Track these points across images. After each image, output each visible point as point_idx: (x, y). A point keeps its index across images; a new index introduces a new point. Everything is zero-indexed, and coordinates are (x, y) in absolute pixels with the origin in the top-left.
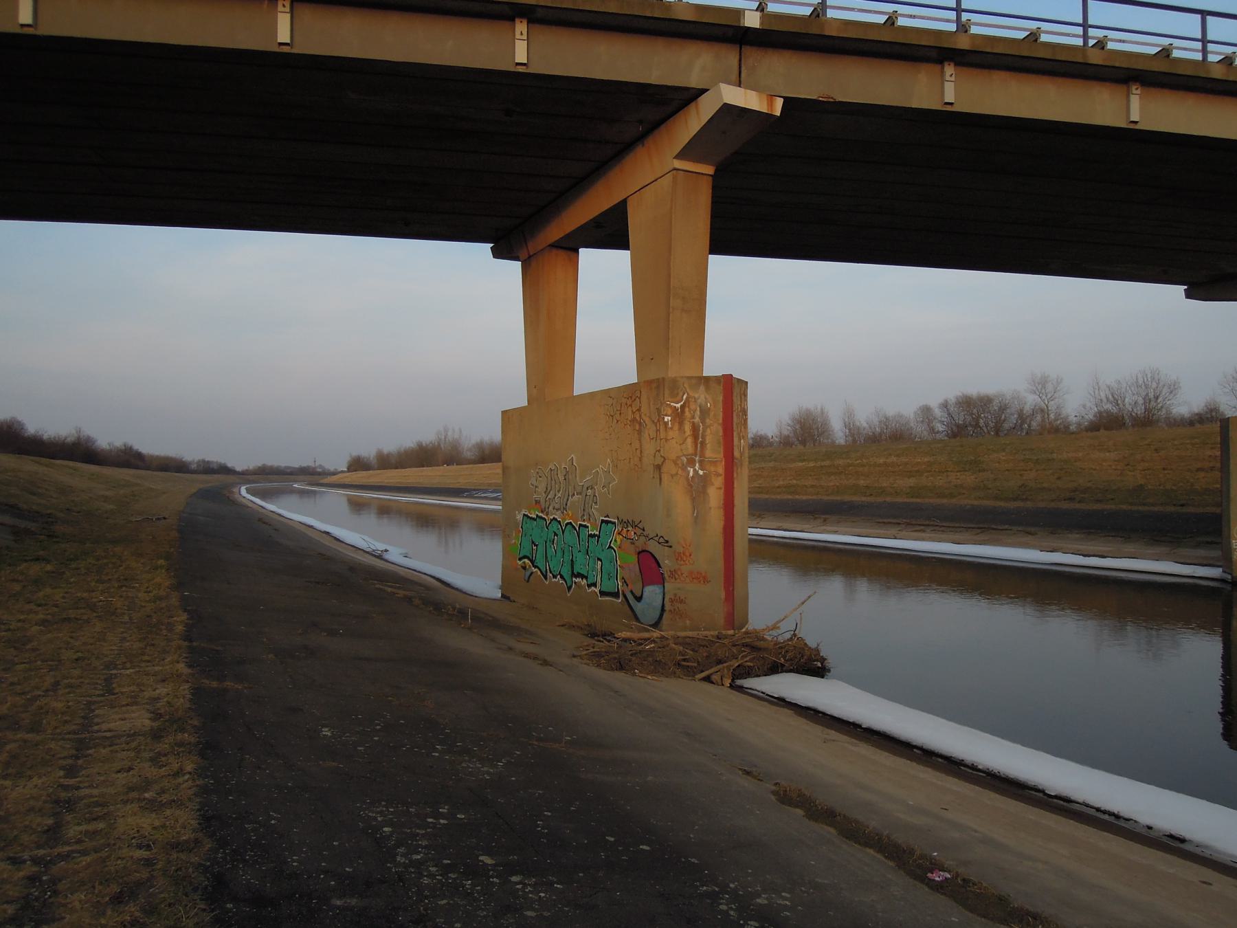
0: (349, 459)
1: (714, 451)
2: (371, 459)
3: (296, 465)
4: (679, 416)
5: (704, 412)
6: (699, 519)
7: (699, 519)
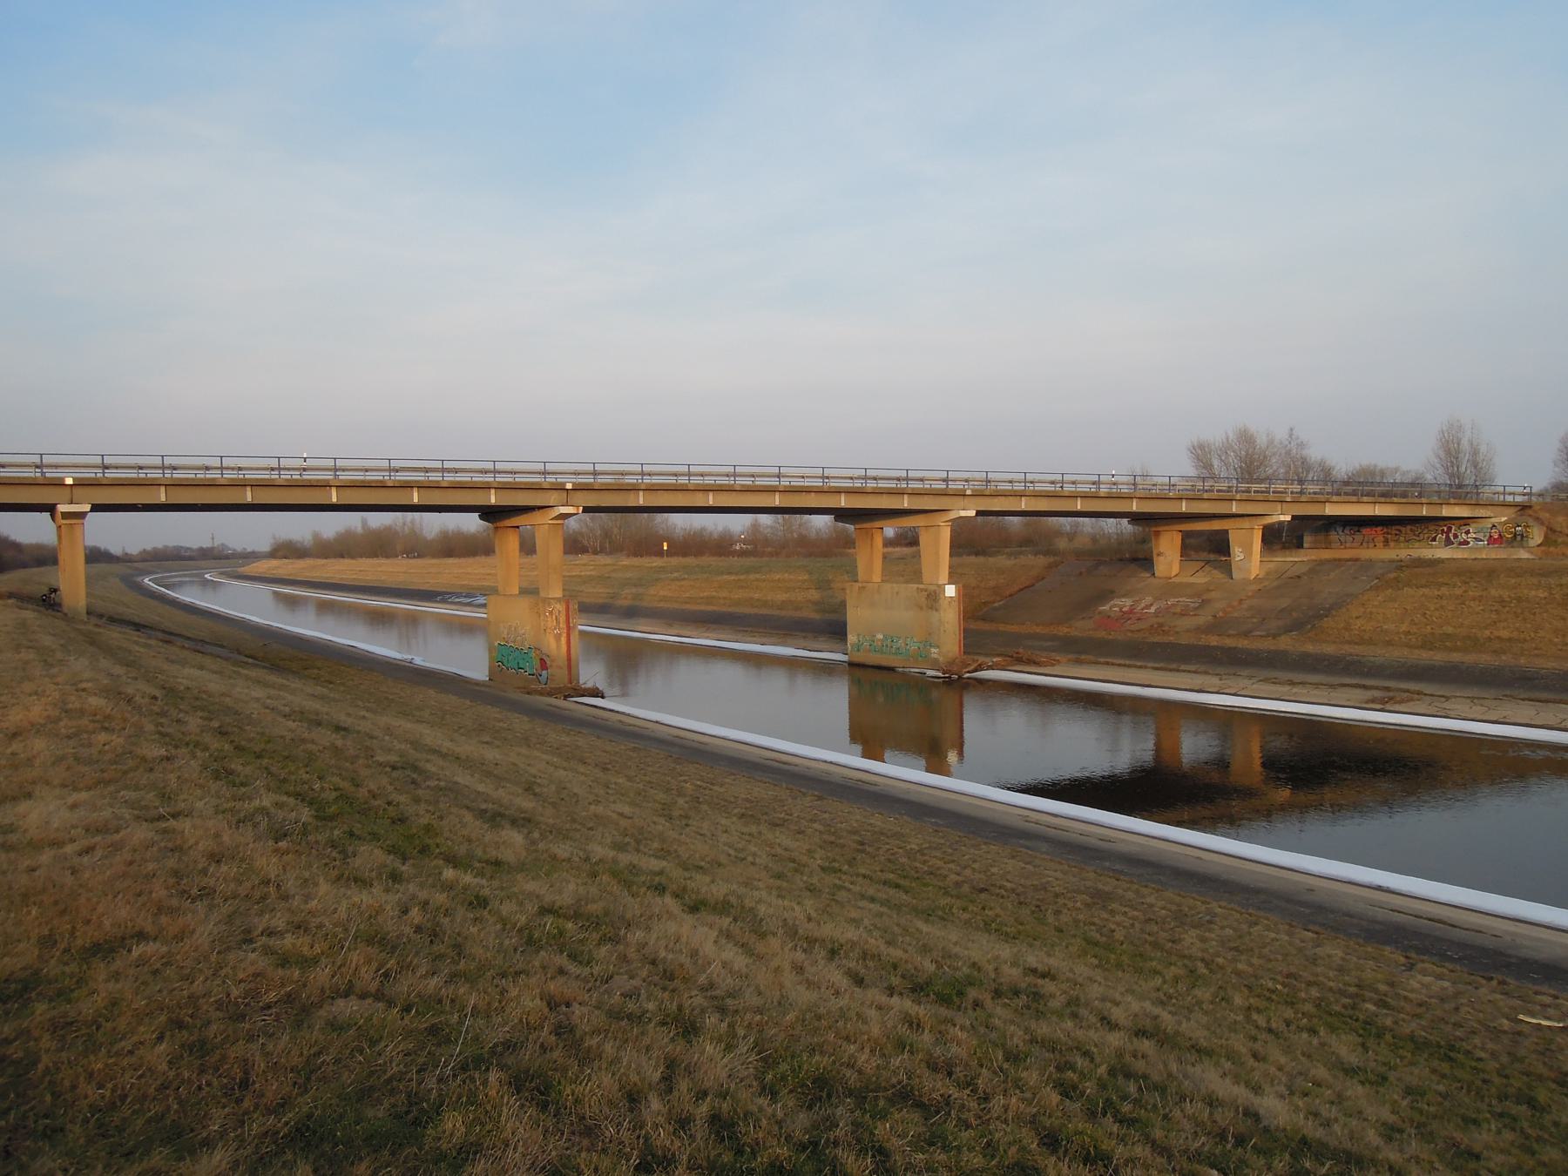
0: (272, 541)
1: (563, 625)
4: (551, 613)
6: (558, 646)
7: (558, 646)
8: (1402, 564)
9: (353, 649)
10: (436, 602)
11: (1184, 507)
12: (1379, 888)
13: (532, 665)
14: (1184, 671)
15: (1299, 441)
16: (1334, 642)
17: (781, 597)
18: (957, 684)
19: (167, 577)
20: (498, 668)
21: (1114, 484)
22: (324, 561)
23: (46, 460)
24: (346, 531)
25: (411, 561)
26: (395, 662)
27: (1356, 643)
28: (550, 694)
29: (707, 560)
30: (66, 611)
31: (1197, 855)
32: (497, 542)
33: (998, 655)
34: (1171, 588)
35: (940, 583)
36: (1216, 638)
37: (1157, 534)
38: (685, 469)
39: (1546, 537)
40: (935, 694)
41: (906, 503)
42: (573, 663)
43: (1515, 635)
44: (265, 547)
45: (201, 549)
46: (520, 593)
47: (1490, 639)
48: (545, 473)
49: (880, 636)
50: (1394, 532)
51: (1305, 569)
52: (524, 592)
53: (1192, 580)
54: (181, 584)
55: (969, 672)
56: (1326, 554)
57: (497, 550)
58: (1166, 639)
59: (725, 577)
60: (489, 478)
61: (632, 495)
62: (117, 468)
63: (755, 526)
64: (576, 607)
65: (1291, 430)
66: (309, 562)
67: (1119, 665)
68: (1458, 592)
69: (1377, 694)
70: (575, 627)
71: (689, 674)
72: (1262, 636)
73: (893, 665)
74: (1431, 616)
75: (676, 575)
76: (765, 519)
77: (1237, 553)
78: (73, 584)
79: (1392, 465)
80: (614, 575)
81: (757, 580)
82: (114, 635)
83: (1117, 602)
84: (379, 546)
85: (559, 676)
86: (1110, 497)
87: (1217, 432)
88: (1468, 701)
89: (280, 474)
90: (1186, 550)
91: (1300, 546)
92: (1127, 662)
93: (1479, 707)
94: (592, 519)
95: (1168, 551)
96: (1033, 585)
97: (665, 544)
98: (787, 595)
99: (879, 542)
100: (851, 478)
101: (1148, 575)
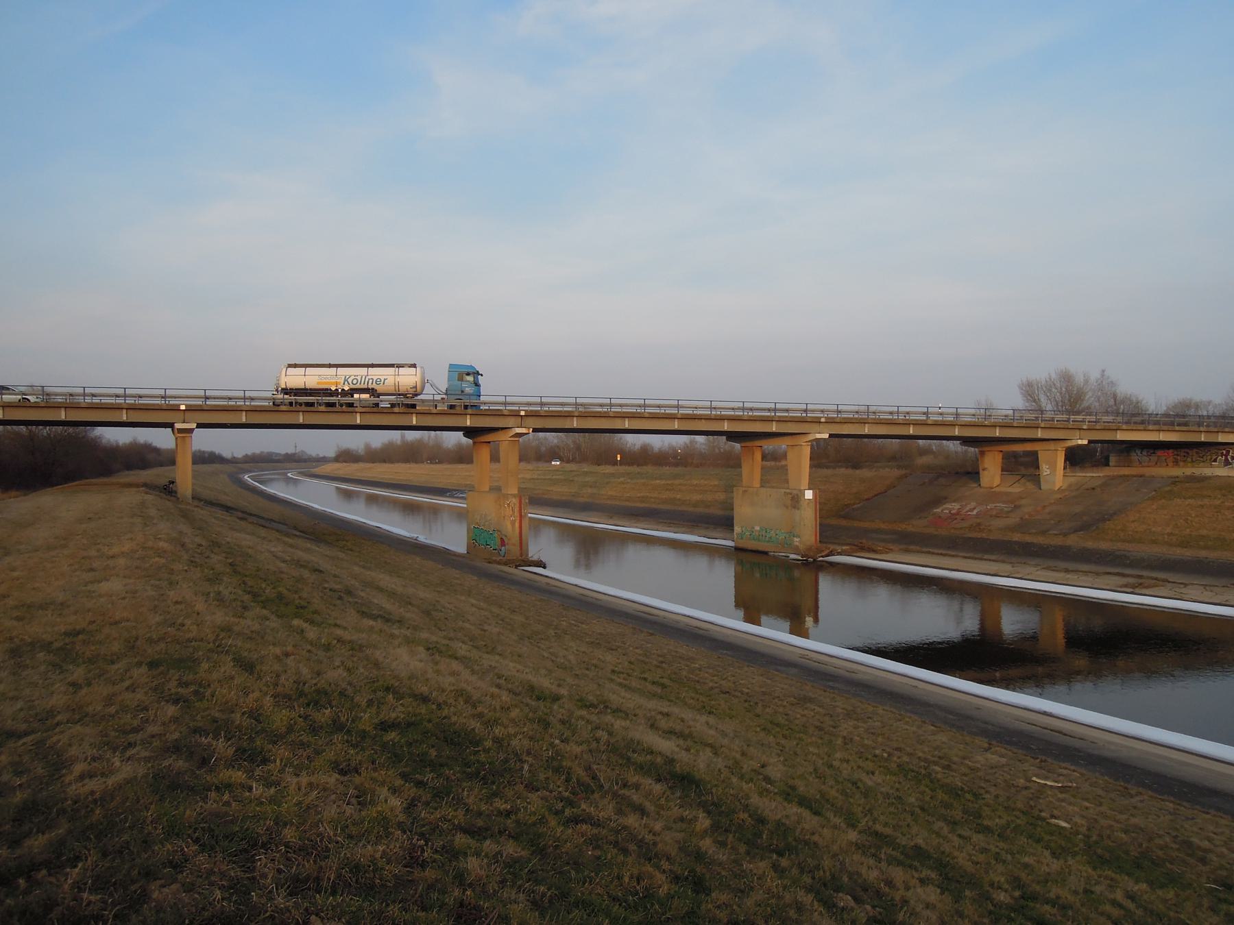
1: (517, 514)
2: (360, 451)
3: (283, 452)
5: (515, 504)
8: (1177, 480)
9: (379, 530)
10: (447, 496)
11: (998, 433)
12: (1045, 713)
14: (986, 560)
15: (1110, 380)
16: (1111, 540)
17: (696, 497)
18: (813, 565)
19: (263, 475)
20: (472, 545)
21: (941, 414)
22: (371, 465)
24: (389, 443)
25: (432, 466)
26: (405, 539)
27: (1128, 542)
28: (506, 564)
29: (649, 469)
30: (179, 496)
31: (914, 684)
32: (474, 455)
34: (993, 496)
35: (802, 488)
37: (982, 453)
38: (608, 401)
40: (796, 573)
41: (774, 428)
42: (524, 542)
44: (331, 454)
46: (490, 489)
49: (757, 528)
50: (1182, 454)
52: (492, 489)
53: (1010, 490)
54: (272, 480)
55: (822, 557)
56: (1126, 471)
57: (474, 459)
58: (979, 535)
59: (658, 481)
60: (120, 401)
62: (214, 398)
63: (691, 442)
64: (527, 501)
65: (1103, 371)
66: (361, 465)
67: (938, 554)
68: (1218, 502)
69: (1131, 580)
70: (526, 514)
71: (634, 554)
72: (1056, 535)
73: (766, 550)
74: (1191, 521)
75: (622, 479)
76: (700, 439)
77: (1045, 470)
78: (185, 477)
80: (576, 479)
82: (202, 513)
83: (948, 506)
84: (410, 454)
85: (514, 551)
86: (936, 424)
87: (1042, 372)
88: (1202, 588)
89: (125, 400)
91: (1107, 465)
92: (944, 552)
93: (1210, 593)
94: (566, 436)
95: (992, 469)
96: (886, 492)
97: (619, 456)
98: (701, 496)
99: (758, 456)
100: (733, 409)
101: (976, 485)
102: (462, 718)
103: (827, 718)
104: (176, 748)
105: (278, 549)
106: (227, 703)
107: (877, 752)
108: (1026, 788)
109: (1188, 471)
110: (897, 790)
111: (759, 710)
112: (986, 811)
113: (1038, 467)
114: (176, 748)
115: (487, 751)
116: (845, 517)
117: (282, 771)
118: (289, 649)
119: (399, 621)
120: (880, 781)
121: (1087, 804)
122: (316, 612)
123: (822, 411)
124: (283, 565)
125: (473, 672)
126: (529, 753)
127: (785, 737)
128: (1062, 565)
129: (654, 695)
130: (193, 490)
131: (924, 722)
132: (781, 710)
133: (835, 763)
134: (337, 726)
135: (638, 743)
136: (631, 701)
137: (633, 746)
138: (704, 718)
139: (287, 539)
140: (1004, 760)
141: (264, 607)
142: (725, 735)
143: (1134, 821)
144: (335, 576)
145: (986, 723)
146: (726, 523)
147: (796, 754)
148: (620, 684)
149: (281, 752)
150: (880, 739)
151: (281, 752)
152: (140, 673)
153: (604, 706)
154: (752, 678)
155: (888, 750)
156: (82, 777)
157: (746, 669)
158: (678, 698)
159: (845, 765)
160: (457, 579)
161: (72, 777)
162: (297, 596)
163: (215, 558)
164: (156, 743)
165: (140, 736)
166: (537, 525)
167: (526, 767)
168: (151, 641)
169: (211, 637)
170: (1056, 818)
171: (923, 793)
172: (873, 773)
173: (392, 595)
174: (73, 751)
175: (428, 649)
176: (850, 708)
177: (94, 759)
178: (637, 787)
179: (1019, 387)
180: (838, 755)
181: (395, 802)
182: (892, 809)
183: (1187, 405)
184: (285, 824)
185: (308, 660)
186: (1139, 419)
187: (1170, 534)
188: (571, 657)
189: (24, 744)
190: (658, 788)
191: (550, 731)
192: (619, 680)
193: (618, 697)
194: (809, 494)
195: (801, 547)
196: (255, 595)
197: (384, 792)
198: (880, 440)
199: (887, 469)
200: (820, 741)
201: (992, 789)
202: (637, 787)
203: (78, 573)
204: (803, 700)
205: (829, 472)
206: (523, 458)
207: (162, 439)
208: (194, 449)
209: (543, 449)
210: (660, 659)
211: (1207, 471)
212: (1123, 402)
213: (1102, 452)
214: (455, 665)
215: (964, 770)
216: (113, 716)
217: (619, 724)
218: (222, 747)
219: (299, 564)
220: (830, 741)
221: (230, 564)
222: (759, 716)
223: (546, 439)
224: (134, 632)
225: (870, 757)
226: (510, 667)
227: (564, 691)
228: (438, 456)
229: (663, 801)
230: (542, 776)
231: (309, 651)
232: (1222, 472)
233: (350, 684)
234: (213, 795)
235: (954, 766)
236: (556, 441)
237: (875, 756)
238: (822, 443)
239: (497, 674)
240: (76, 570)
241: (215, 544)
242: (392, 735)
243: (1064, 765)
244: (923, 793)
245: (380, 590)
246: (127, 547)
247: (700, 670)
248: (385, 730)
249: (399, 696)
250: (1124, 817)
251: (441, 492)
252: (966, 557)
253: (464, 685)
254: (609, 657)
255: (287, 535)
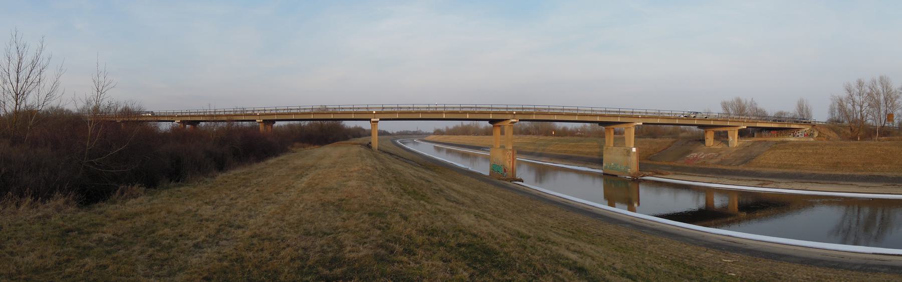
0: (434, 129)
1: (511, 158)
3: (412, 130)
4: (508, 154)
11: (712, 123)
13: (502, 171)
17: (588, 150)
18: (636, 181)
23: (369, 106)
28: (506, 180)
29: (568, 138)
33: (651, 172)
34: (710, 150)
36: (721, 166)
37: (706, 132)
39: (819, 134)
40: (630, 184)
41: (619, 120)
43: (802, 163)
44: (432, 131)
45: (414, 132)
47: (796, 165)
48: (507, 108)
49: (613, 164)
51: (750, 144)
53: (717, 147)
54: (408, 142)
56: (760, 139)
60: (352, 110)
61: (531, 116)
63: (584, 126)
65: (752, 99)
66: (444, 136)
68: (791, 151)
69: (761, 182)
71: (560, 176)
75: (556, 143)
76: (588, 125)
77: (730, 139)
78: (375, 140)
79: (787, 111)
80: (537, 142)
81: (581, 145)
82: (382, 156)
83: (692, 154)
84: (465, 131)
85: (510, 174)
87: (730, 98)
90: (716, 138)
99: (612, 132)
100: (601, 111)
102: (491, 244)
103: (642, 244)
104: (381, 246)
105: (412, 172)
106: (399, 231)
107: (663, 256)
108: (720, 264)
109: (781, 139)
110: (670, 269)
111: (614, 242)
112: (705, 274)
113: (728, 138)
114: (381, 246)
115: (502, 257)
116: (650, 160)
117: (421, 259)
118: (421, 212)
119: (462, 204)
120: (663, 267)
121: (741, 266)
122: (429, 198)
123: (640, 113)
124: (414, 178)
125: (494, 226)
126: (518, 259)
127: (624, 252)
128: (736, 177)
129: (569, 237)
130: (378, 146)
131: (681, 243)
132: (623, 241)
133: (645, 262)
134: (441, 244)
135: (562, 255)
136: (559, 239)
137: (560, 256)
138: (590, 246)
139: (415, 168)
140: (712, 255)
141: (409, 195)
142: (598, 252)
143: (758, 269)
144: (435, 184)
145: (705, 241)
146: (599, 162)
147: (629, 259)
148: (554, 232)
149: (420, 252)
150: (664, 251)
151: (420, 252)
152: (365, 217)
153: (548, 241)
154: (610, 229)
155: (667, 255)
156: (350, 252)
157: (608, 225)
158: (579, 238)
159: (649, 262)
160: (485, 186)
161: (347, 251)
162: (421, 191)
163: (389, 174)
164: (374, 243)
165: (368, 240)
166: (520, 163)
167: (517, 264)
168: (368, 205)
169: (390, 206)
170: (731, 273)
171: (680, 270)
172: (660, 264)
173: (459, 192)
174: (346, 242)
175: (475, 215)
176: (652, 240)
177: (353, 246)
178: (562, 272)
179: (722, 104)
180: (646, 258)
181: (465, 274)
182: (667, 277)
183: (781, 113)
184: (424, 278)
185: (428, 217)
186: (765, 118)
187: (775, 164)
188: (534, 221)
189: (330, 237)
190: (570, 273)
191: (527, 250)
192: (554, 231)
193: (553, 237)
194: (634, 150)
195: (632, 173)
196: (405, 190)
197: (461, 270)
198: (665, 126)
199: (667, 139)
200: (639, 253)
201: (707, 266)
202: (562, 272)
203: (341, 177)
204: (632, 238)
205: (644, 139)
206: (514, 133)
207: (366, 125)
208: (379, 129)
209: (523, 129)
210: (572, 222)
211: (787, 139)
212: (759, 111)
213: (752, 132)
214: (487, 223)
215: (697, 260)
216: (358, 232)
217: (554, 248)
218: (398, 248)
219: (421, 178)
220: (643, 253)
221: (395, 177)
222: (614, 244)
223: (524, 124)
224: (362, 202)
225: (660, 258)
226: (509, 224)
227: (531, 235)
228: (477, 132)
229: (572, 277)
230: (523, 268)
231: (428, 214)
232: (792, 139)
233: (445, 228)
234: (396, 264)
235: (693, 259)
236: (528, 125)
237: (662, 257)
238: (640, 127)
239: (504, 227)
240: (339, 176)
241: (388, 169)
242: (463, 249)
243: (734, 254)
244: (680, 270)
245: (454, 190)
246: (356, 168)
247: (588, 226)
248: (460, 247)
249: (465, 234)
250: (754, 269)
251: (478, 148)
252: (699, 176)
253: (491, 231)
254: (550, 221)
255: (415, 166)
